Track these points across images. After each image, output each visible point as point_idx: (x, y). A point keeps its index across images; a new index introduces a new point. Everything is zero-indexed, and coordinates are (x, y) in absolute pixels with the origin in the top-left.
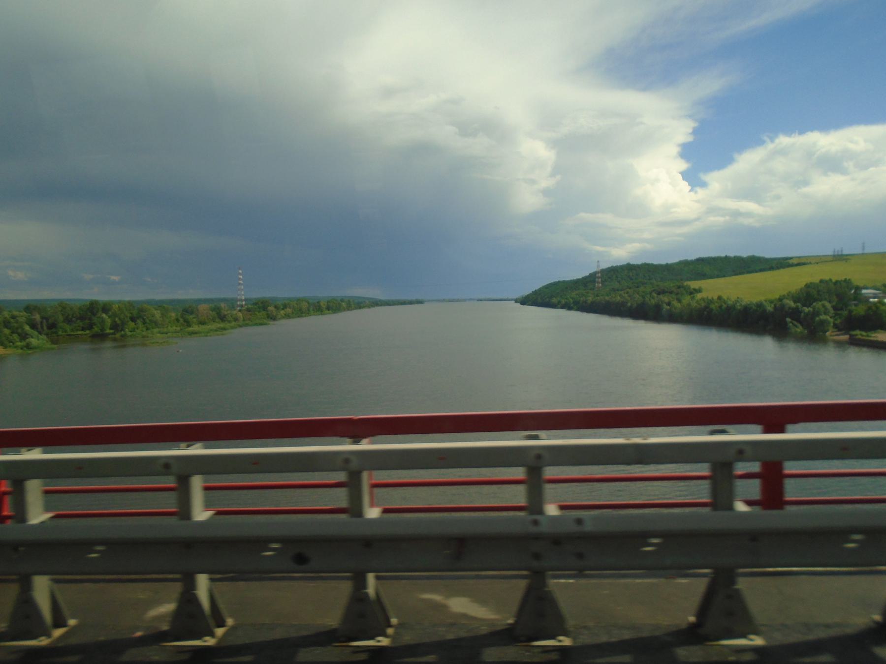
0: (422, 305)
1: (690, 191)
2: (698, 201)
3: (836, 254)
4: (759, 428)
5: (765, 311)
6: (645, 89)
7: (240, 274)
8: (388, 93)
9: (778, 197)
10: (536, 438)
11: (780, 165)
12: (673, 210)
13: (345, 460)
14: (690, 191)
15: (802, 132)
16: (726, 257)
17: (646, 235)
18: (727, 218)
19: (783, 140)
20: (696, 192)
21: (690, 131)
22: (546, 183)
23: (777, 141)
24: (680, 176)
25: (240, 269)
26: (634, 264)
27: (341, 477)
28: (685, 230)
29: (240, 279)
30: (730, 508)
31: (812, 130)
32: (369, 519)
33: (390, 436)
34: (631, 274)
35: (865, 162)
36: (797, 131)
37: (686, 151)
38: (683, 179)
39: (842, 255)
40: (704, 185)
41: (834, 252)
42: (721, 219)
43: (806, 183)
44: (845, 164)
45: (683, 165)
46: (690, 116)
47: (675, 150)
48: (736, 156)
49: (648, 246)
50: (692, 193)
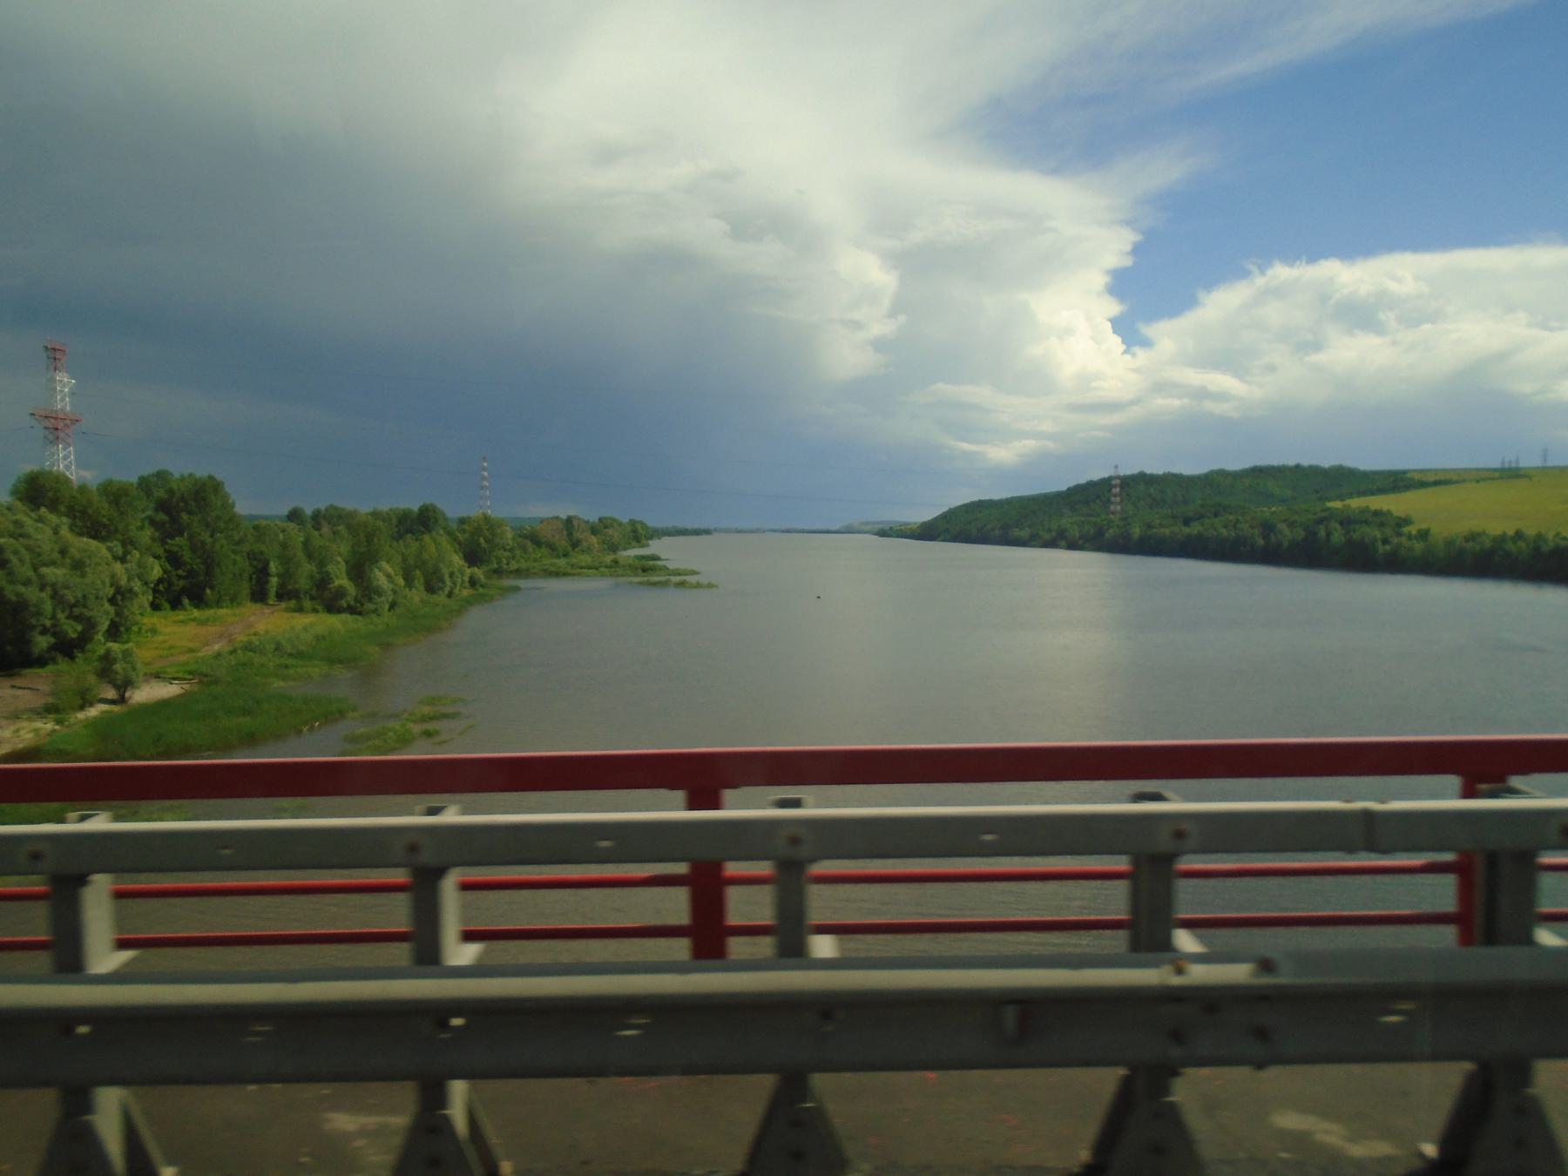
0: (708, 536)
1: (1125, 352)
2: (1137, 370)
3: (1507, 466)
4: (679, 796)
5: (329, 584)
6: (1054, 172)
7: (484, 469)
8: (608, 155)
9: (1271, 368)
10: (1157, 797)
11: (1273, 313)
12: (1094, 384)
13: (413, 840)
14: (1125, 352)
15: (1313, 259)
16: (1298, 467)
17: (1046, 427)
18: (1186, 401)
19: (1281, 272)
20: (1134, 355)
21: (1128, 248)
22: (880, 328)
23: (1270, 272)
24: (1109, 324)
25: (484, 459)
26: (1104, 478)
27: (399, 876)
28: (1115, 419)
29: (484, 478)
30: (1529, 940)
31: (1326, 257)
32: (96, 975)
33: (640, 790)
34: (1152, 490)
35: (1416, 314)
36: (1304, 258)
37: (1120, 284)
38: (1114, 332)
39: (1518, 469)
40: (1146, 343)
41: (1503, 463)
42: (1176, 403)
43: (1317, 346)
44: (1382, 316)
45: (1113, 308)
46: (1128, 223)
47: (1100, 280)
48: (1202, 295)
49: (1050, 445)
50: (1128, 357)
